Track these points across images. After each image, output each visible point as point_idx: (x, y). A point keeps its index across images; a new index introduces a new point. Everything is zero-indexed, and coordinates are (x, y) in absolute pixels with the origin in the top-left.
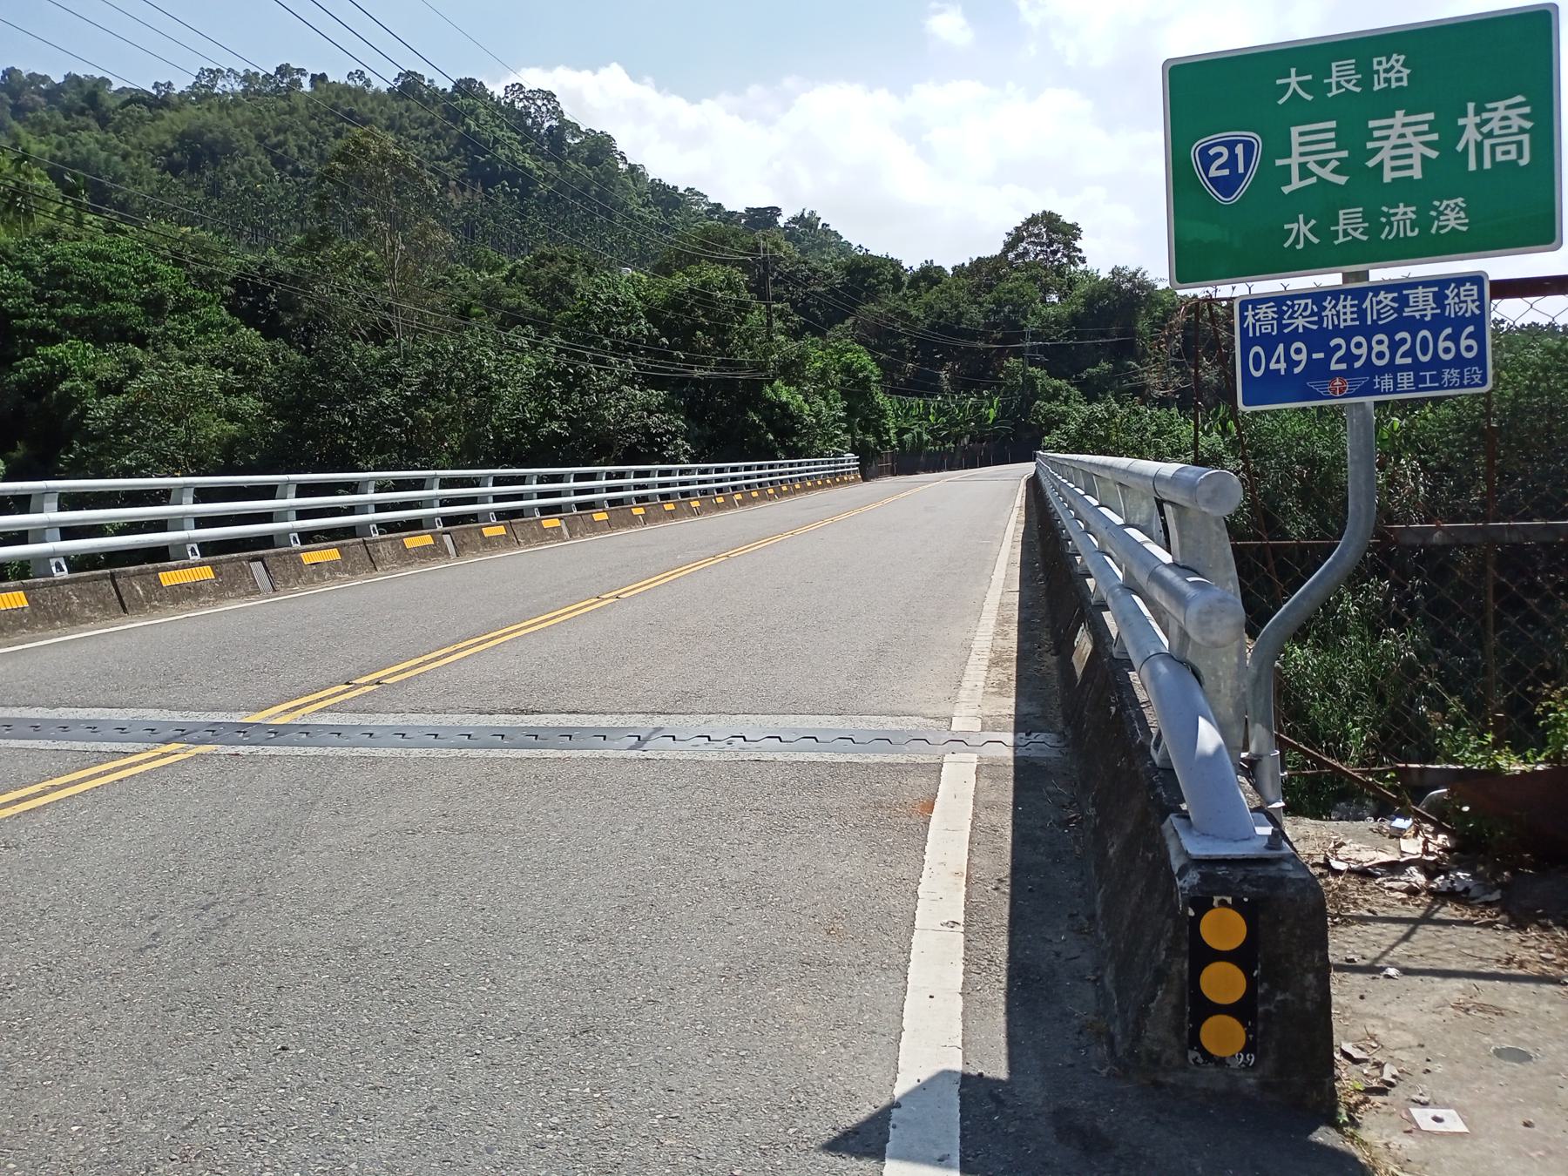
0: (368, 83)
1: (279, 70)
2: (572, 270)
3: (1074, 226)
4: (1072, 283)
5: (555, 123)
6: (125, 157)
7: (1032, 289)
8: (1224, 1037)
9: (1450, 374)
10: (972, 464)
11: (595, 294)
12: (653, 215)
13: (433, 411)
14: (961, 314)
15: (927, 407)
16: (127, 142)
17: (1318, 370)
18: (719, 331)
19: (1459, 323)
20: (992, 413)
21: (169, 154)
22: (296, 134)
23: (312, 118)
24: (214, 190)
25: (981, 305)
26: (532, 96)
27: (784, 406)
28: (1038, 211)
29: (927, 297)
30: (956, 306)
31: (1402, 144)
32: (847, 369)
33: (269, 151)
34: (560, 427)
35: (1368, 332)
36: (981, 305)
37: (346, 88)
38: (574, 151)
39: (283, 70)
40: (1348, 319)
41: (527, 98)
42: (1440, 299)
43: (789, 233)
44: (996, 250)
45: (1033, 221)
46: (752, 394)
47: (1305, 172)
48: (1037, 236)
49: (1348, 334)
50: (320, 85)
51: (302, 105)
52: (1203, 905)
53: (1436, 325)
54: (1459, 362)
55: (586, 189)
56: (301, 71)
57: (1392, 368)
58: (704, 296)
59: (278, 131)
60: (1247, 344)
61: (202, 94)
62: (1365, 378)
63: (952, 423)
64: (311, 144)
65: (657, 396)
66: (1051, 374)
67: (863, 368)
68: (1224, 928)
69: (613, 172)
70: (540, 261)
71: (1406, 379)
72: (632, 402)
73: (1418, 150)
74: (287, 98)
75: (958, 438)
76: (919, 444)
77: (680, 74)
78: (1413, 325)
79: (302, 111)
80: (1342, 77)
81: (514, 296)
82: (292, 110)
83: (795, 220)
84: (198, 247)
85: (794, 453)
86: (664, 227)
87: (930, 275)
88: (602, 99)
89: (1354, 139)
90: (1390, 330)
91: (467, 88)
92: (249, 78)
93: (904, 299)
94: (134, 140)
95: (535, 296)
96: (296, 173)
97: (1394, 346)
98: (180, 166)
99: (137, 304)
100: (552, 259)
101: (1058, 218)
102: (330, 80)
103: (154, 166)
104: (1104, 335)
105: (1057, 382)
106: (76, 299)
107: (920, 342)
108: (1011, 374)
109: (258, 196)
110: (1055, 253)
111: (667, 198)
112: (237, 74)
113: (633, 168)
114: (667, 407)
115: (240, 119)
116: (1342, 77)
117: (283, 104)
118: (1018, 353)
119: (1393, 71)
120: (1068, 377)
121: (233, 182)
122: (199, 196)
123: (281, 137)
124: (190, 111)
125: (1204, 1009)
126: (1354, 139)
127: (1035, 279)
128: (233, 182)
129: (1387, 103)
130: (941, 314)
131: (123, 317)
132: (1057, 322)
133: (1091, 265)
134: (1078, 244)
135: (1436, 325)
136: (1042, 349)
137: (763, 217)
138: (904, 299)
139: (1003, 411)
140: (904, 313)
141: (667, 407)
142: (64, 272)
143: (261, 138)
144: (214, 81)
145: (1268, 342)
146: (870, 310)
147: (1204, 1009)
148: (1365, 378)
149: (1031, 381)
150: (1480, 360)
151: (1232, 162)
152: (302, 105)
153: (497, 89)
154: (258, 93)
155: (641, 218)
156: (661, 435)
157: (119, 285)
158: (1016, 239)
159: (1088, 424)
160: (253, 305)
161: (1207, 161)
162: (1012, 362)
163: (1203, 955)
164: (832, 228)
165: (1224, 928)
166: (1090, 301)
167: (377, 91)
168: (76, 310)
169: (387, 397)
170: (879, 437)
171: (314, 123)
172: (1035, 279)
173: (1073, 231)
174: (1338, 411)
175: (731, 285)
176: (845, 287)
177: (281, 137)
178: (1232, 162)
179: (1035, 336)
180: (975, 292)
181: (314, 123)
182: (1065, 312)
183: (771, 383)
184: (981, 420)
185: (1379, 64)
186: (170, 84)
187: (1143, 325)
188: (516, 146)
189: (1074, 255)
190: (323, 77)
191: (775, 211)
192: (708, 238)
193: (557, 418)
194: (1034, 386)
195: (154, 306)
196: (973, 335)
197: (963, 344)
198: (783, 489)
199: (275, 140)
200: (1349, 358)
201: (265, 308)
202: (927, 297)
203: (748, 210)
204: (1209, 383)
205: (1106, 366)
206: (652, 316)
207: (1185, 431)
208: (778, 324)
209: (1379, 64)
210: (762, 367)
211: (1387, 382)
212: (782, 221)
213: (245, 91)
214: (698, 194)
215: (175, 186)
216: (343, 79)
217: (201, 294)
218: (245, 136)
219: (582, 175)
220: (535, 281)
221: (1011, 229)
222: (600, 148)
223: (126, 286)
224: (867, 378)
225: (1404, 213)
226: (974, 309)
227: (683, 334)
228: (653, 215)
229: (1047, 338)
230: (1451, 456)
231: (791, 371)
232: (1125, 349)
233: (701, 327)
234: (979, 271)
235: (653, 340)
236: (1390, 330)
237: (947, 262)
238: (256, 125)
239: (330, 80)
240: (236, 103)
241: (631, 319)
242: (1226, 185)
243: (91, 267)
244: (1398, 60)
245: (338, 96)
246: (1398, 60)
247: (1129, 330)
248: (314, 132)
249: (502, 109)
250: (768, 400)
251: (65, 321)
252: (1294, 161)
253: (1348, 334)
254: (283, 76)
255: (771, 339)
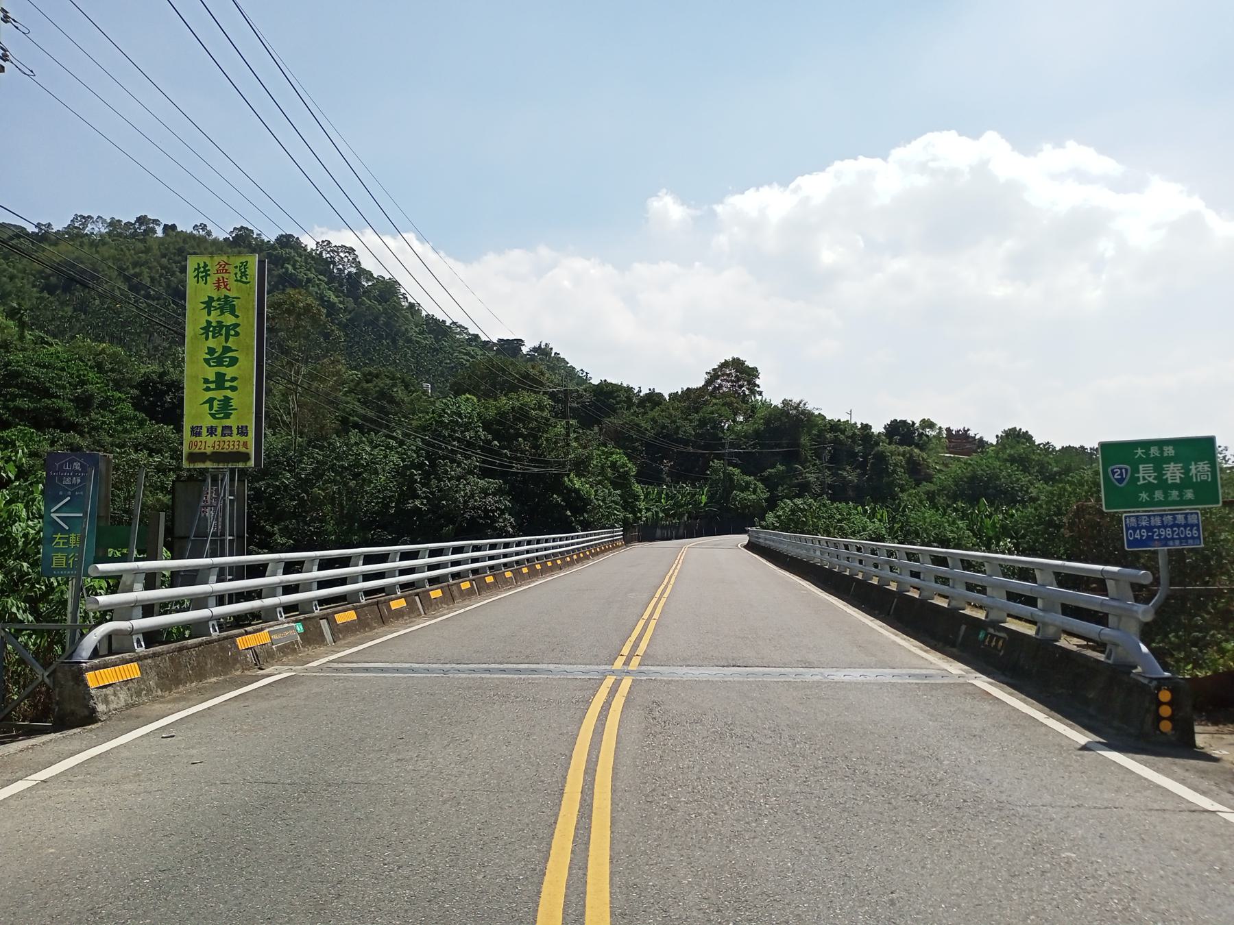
0: (209, 233)
1: (138, 219)
2: (394, 385)
3: (755, 369)
4: (754, 408)
5: (354, 270)
6: (12, 278)
7: (726, 411)
8: (1166, 726)
9: (1190, 541)
10: (691, 535)
11: (443, 410)
12: (429, 341)
13: (323, 490)
14: (678, 428)
15: (660, 494)
16: (14, 267)
17: (1150, 538)
18: (534, 437)
19: (1192, 526)
20: (704, 499)
21: (47, 278)
22: (149, 268)
23: (164, 256)
24: (82, 307)
25: (691, 421)
26: (336, 250)
27: (577, 491)
28: (729, 358)
29: (651, 414)
30: (675, 422)
31: (1173, 472)
32: (614, 466)
33: (127, 279)
34: (422, 503)
35: (1165, 527)
36: (691, 421)
37: (191, 236)
38: (367, 291)
39: (142, 220)
40: (1159, 523)
41: (333, 251)
42: (1186, 518)
43: (530, 358)
44: (701, 383)
45: (725, 364)
46: (556, 483)
47: (1144, 479)
48: (728, 375)
49: (1159, 527)
50: (171, 232)
51: (155, 247)
52: (1159, 689)
53: (1185, 526)
54: (1193, 538)
55: (377, 319)
56: (156, 222)
57: (1173, 539)
58: (522, 414)
59: (135, 264)
60: (1127, 529)
61: (74, 234)
62: (1165, 541)
63: (677, 505)
64: (161, 276)
65: (493, 483)
66: (744, 472)
67: (624, 465)
68: (1165, 696)
69: (397, 307)
70: (368, 378)
71: (1177, 542)
72: (472, 488)
73: (1178, 475)
74: (144, 241)
75: (681, 516)
76: (656, 521)
77: (460, 240)
78: (1178, 526)
79: (156, 251)
80: (1154, 451)
81: (347, 403)
82: (148, 250)
83: (535, 350)
84: (114, 357)
85: (586, 526)
86: (435, 350)
87: (653, 399)
88: (380, 253)
89: (1159, 470)
90: (1172, 527)
91: (287, 241)
92: (114, 224)
93: (635, 414)
94: (20, 266)
95: (364, 403)
96: (148, 296)
97: (1173, 532)
98: (56, 287)
99: (70, 400)
100: (377, 376)
101: (743, 363)
102: (179, 229)
103: (34, 286)
104: (778, 446)
105: (747, 478)
106: (23, 396)
107: (648, 446)
108: (715, 471)
109: (118, 313)
110: (741, 387)
111: (437, 328)
112: (104, 221)
113: (412, 306)
114: (499, 492)
115: (107, 255)
116: (1154, 451)
117: (140, 246)
118: (719, 457)
119: (1169, 451)
120: (755, 475)
121: (97, 302)
122: (69, 310)
123: (137, 270)
124: (63, 247)
125: (1160, 719)
126: (1159, 470)
127: (730, 405)
128: (97, 302)
129: (1169, 460)
130: (664, 427)
131: (60, 410)
132: (745, 437)
133: (767, 396)
134: (758, 382)
135: (1185, 526)
136: (737, 455)
137: (512, 346)
138: (635, 414)
139: (711, 498)
140: (638, 425)
141: (499, 492)
142: (16, 375)
143: (121, 270)
144: (85, 225)
145: (1134, 529)
146: (613, 421)
147: (1160, 719)
148: (1165, 541)
149: (730, 476)
150: (1199, 537)
151: (1121, 474)
152: (155, 247)
153: (310, 243)
154: (120, 235)
155: (418, 342)
156: (492, 511)
157: (57, 385)
158: (714, 375)
159: (793, 511)
160: (154, 404)
161: (1114, 473)
162: (716, 463)
163: (1160, 703)
164: (562, 356)
165: (1165, 696)
166: (767, 421)
167: (216, 240)
168: (24, 403)
169: (287, 478)
170: (635, 515)
171: (164, 261)
172: (730, 405)
173: (752, 373)
174: (1155, 552)
175: (541, 407)
176: (592, 404)
177: (137, 270)
178: (1121, 474)
179: (732, 445)
180: (686, 414)
181: (164, 261)
182: (749, 428)
183: (568, 475)
184: (697, 503)
185: (1165, 448)
186: (49, 224)
187: (805, 440)
188: (323, 286)
189: (753, 385)
190: (174, 227)
191: (520, 342)
192: (493, 365)
193: (418, 497)
194: (732, 480)
195: (84, 403)
196: (686, 442)
197: (678, 448)
198: (582, 555)
199: (132, 272)
200: (1160, 535)
201: (162, 406)
202: (651, 414)
203: (500, 340)
204: (851, 481)
205: (782, 468)
206: (487, 426)
207: (859, 520)
208: (573, 435)
209: (1165, 448)
210: (563, 465)
211: (1171, 543)
212: (525, 350)
213: (109, 233)
214: (460, 326)
215: (51, 303)
216: (189, 230)
217: (118, 395)
218: (110, 267)
219: (372, 310)
220: (365, 392)
221: (709, 369)
222: (388, 289)
223: (64, 387)
224: (627, 473)
225: (1175, 493)
226: (686, 423)
227: (507, 438)
228: (429, 341)
229: (739, 447)
230: (1036, 541)
231: (581, 467)
232: (792, 456)
233: (522, 435)
234: (689, 398)
235: (488, 442)
236: (1172, 527)
237: (666, 390)
238: (119, 260)
239: (179, 229)
240: (103, 241)
241: (467, 427)
242: (1121, 481)
243: (37, 372)
244: (1171, 448)
245: (185, 241)
246: (1171, 448)
247: (795, 443)
248: (163, 267)
249: (313, 258)
250: (566, 488)
251: (19, 413)
252: (1141, 475)
253: (1159, 527)
254: (141, 224)
255: (568, 445)
